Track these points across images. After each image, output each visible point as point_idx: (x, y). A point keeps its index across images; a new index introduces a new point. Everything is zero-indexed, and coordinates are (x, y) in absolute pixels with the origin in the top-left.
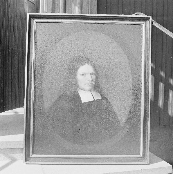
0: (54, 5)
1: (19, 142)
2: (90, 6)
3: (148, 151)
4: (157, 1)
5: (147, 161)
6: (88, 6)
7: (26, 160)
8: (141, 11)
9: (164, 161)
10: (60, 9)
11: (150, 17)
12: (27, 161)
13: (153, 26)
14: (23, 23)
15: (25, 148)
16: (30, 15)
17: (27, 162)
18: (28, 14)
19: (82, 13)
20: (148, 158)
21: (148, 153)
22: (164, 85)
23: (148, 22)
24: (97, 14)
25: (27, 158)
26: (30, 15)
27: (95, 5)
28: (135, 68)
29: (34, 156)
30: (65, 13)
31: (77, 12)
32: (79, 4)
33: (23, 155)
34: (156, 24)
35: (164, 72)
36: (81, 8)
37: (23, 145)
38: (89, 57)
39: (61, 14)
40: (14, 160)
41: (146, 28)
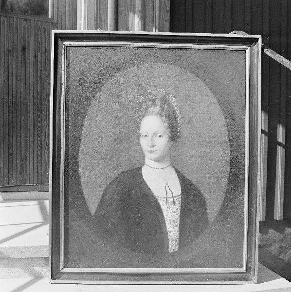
0: (99, 21)
1: (41, 248)
2: (157, 21)
3: (257, 263)
4: (270, 1)
5: (255, 279)
6: (155, 22)
7: (53, 277)
8: (243, 29)
9: (283, 279)
10: (109, 26)
11: (259, 37)
12: (55, 279)
13: (264, 55)
14: (7, 21)
15: (52, 257)
16: (56, 34)
17: (54, 281)
18: (53, 32)
19: (144, 30)
20: (256, 273)
21: (256, 264)
22: (284, 150)
23: (255, 47)
24: (170, 32)
25: (55, 275)
26: (56, 34)
27: (166, 21)
28: (232, 122)
29: (66, 270)
30: (117, 29)
31: (136, 27)
32: (139, 11)
33: (46, 271)
34: (268, 52)
35: (283, 126)
36: (143, 18)
37: (47, 253)
38: (172, 118)
39: (110, 31)
40: (38, 277)
41: (253, 56)
